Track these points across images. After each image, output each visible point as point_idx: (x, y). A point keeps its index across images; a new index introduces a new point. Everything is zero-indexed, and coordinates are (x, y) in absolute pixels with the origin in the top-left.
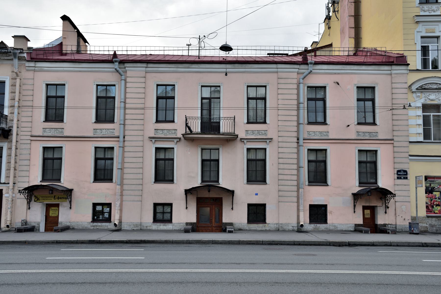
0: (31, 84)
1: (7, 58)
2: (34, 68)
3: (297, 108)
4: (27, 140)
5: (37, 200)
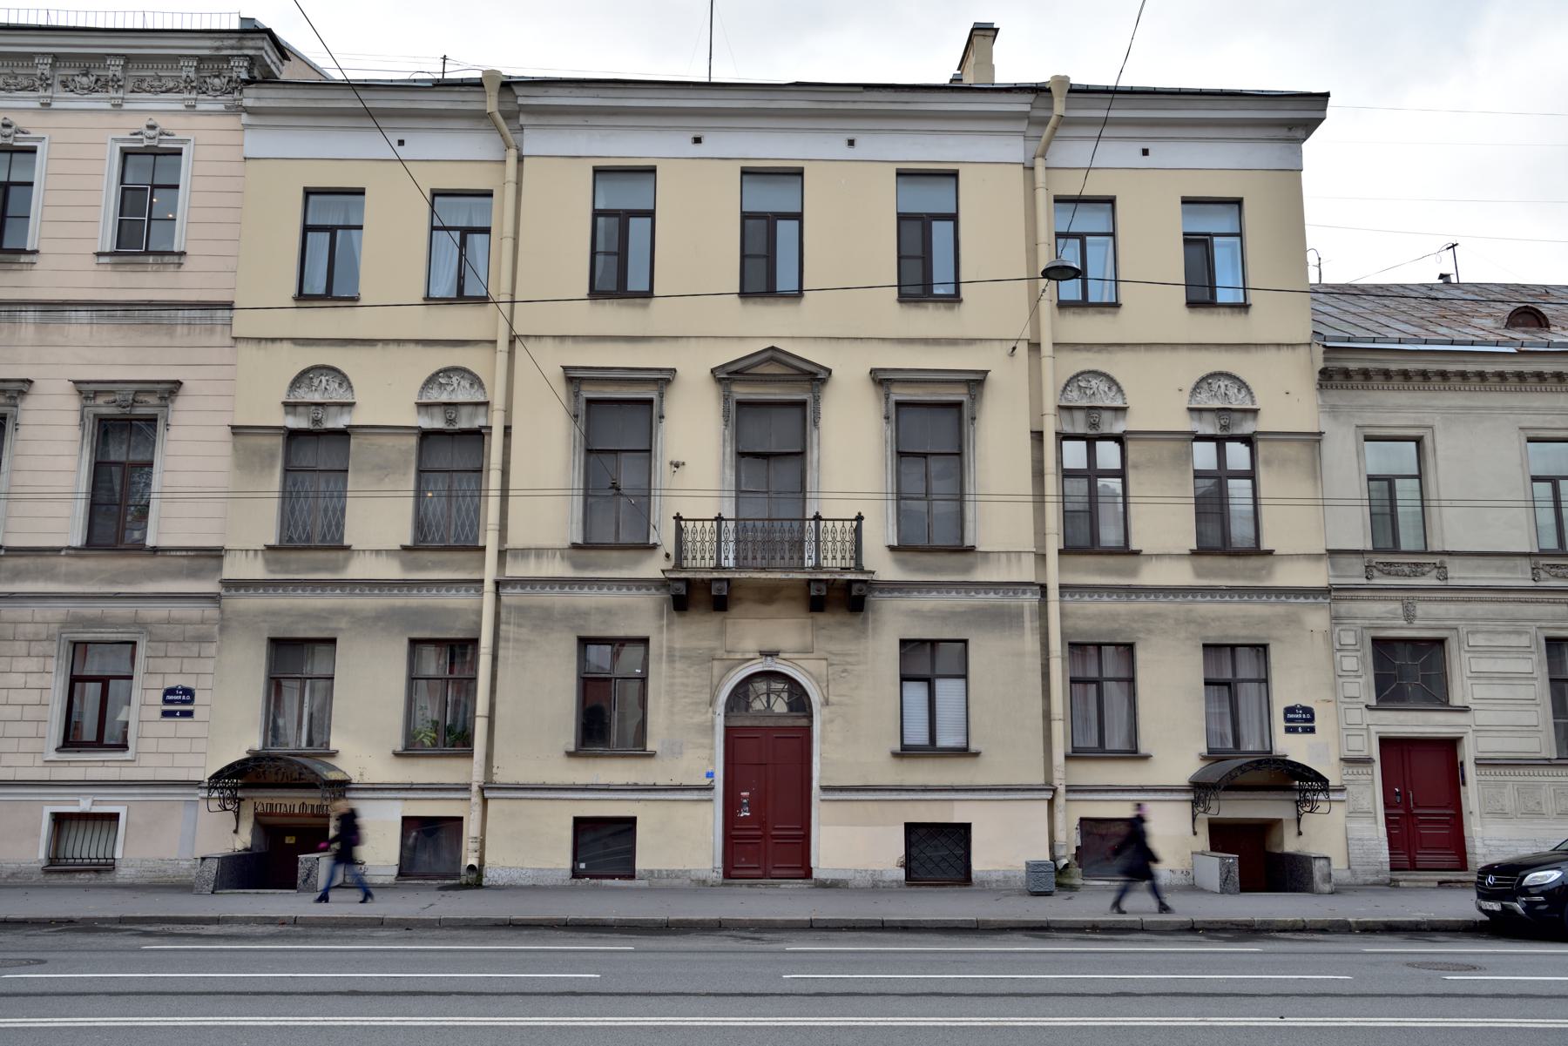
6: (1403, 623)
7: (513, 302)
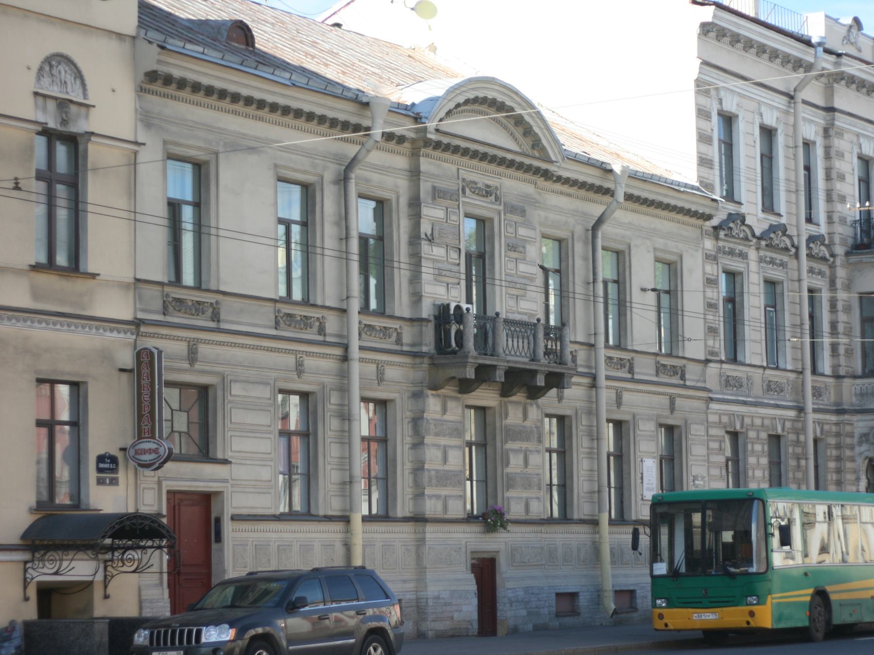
6: (186, 365)
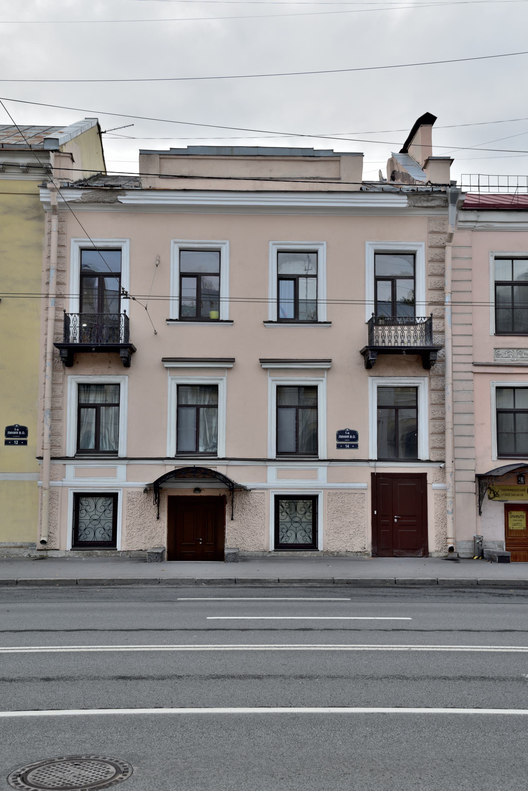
0: (467, 257)
1: (428, 203)
2: (474, 224)
3: (445, 304)
4: (465, 372)
5: (495, 496)
7: (479, 186)
